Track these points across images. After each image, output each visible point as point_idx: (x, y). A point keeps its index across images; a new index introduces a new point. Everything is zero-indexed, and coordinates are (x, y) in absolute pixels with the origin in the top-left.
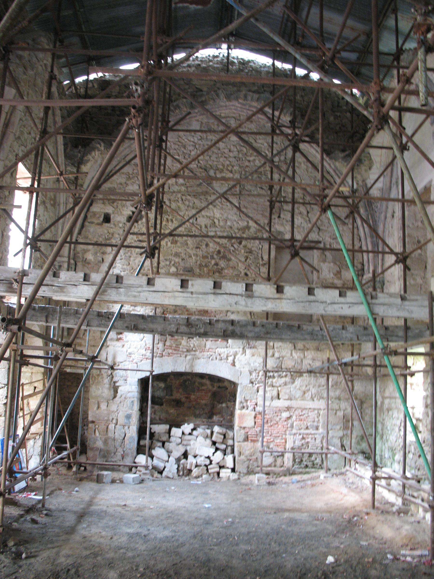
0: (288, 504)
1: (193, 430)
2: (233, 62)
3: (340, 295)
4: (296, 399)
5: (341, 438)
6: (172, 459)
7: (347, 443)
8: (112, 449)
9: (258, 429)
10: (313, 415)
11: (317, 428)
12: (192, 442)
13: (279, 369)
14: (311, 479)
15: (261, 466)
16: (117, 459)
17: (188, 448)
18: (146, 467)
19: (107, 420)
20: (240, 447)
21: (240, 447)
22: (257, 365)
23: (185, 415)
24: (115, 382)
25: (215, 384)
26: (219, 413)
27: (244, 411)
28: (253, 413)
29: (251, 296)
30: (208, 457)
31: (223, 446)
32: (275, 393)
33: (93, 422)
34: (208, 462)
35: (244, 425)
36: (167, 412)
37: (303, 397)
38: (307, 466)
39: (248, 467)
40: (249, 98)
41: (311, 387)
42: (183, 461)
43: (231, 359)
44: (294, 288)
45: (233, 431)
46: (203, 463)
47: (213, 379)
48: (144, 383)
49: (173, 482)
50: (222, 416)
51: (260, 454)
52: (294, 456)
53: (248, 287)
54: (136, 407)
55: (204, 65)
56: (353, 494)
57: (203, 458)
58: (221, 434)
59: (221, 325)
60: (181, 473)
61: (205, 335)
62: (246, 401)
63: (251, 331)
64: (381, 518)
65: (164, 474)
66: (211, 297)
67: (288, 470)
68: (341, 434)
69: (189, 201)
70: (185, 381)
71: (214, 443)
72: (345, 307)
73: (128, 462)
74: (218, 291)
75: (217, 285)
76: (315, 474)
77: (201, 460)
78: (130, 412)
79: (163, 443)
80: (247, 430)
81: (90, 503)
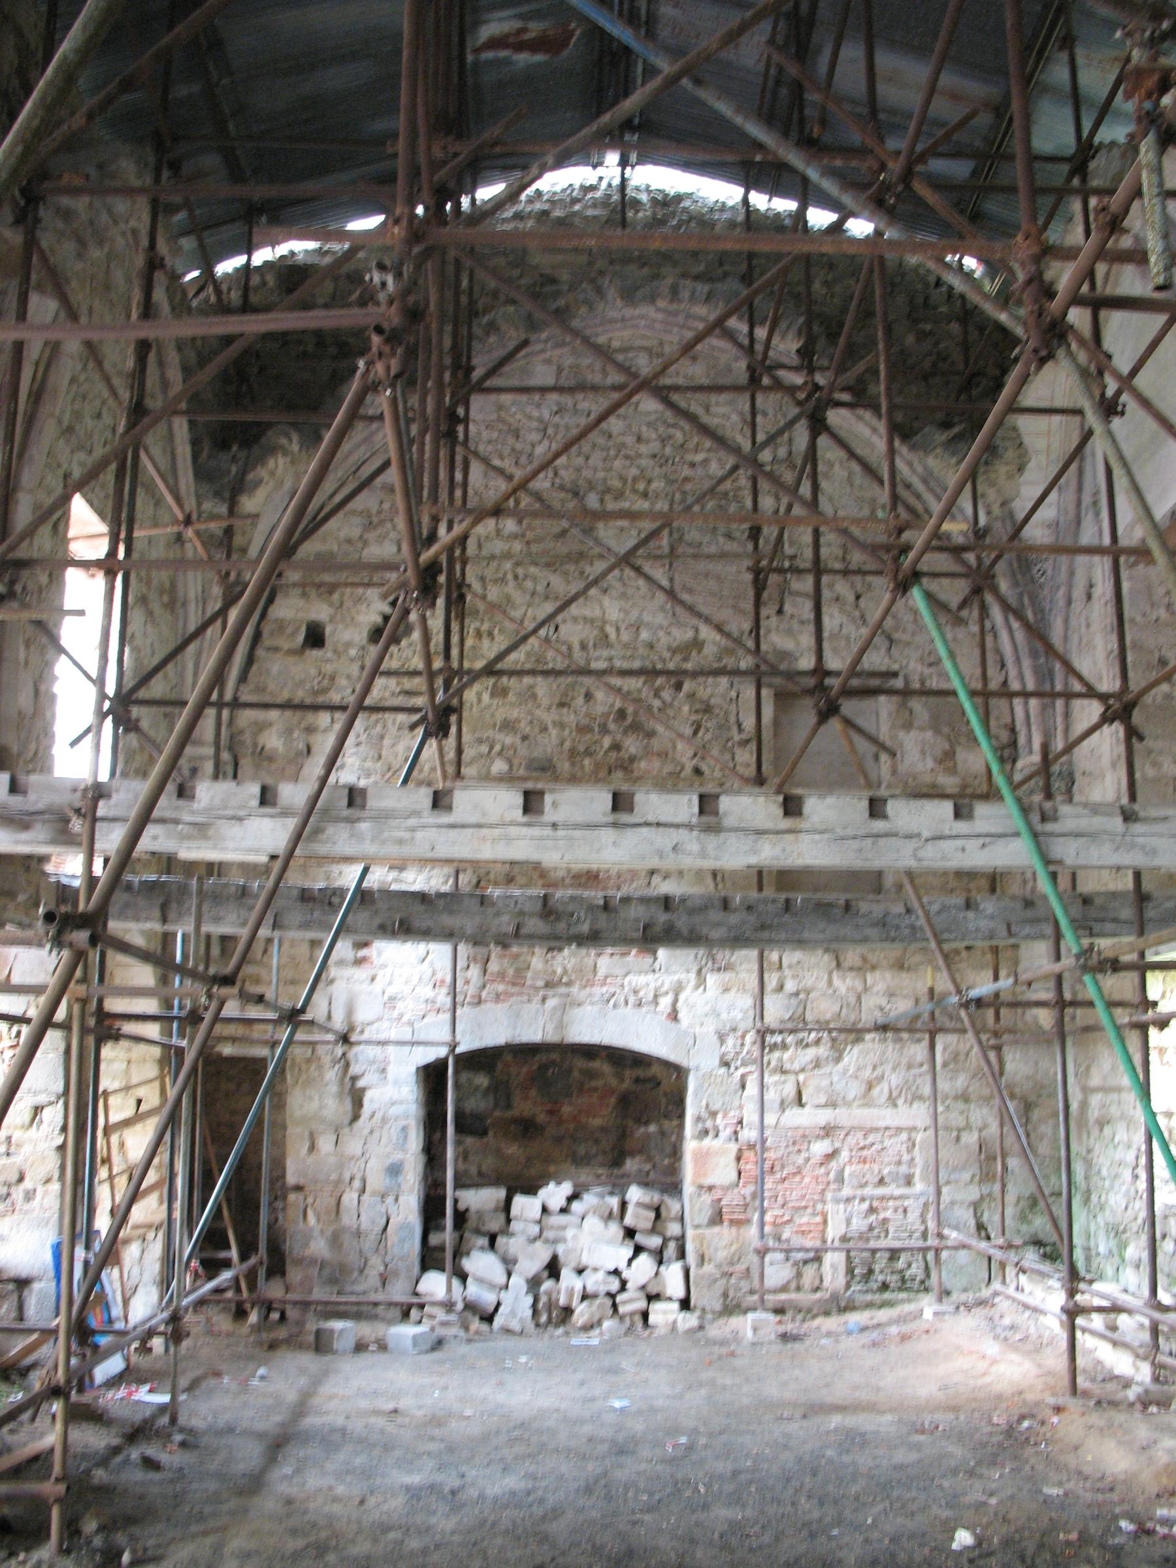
0: (840, 1392)
1: (571, 1199)
3: (958, 815)
4: (848, 1104)
5: (976, 1206)
6: (518, 1282)
8: (353, 1259)
9: (748, 1190)
10: (895, 1145)
11: (909, 1181)
13: (797, 1025)
14: (900, 1320)
16: (366, 1286)
17: (560, 1249)
18: (449, 1306)
19: (338, 1182)
21: (701, 1239)
23: (547, 1160)
24: (354, 1079)
25: (627, 1073)
26: (641, 1150)
27: (708, 1142)
28: (733, 1148)
29: (714, 829)
30: (616, 1272)
31: (657, 1239)
32: (789, 1090)
33: (299, 1188)
34: (615, 1285)
36: (498, 1153)
38: (885, 1287)
39: (725, 1295)
40: (685, 294)
41: (888, 1068)
42: (547, 1285)
43: (665, 1002)
44: (830, 800)
45: (680, 1198)
46: (603, 1289)
48: (432, 1077)
49: (522, 1343)
50: (649, 1159)
51: (755, 1259)
52: (848, 1258)
53: (707, 804)
54: (415, 1141)
55: (558, 213)
56: (1014, 1357)
57: (600, 1275)
58: (647, 1207)
59: (636, 912)
60: (544, 1318)
61: (593, 939)
62: (714, 1114)
63: (718, 925)
65: (498, 1321)
66: (608, 835)
67: (835, 1297)
68: (974, 1193)
69: (535, 579)
70: (543, 1068)
71: (630, 1233)
72: (974, 844)
73: (398, 1292)
74: (624, 818)
75: (621, 803)
76: (908, 1308)
77: (596, 1281)
78: (398, 1156)
81: (301, 1409)
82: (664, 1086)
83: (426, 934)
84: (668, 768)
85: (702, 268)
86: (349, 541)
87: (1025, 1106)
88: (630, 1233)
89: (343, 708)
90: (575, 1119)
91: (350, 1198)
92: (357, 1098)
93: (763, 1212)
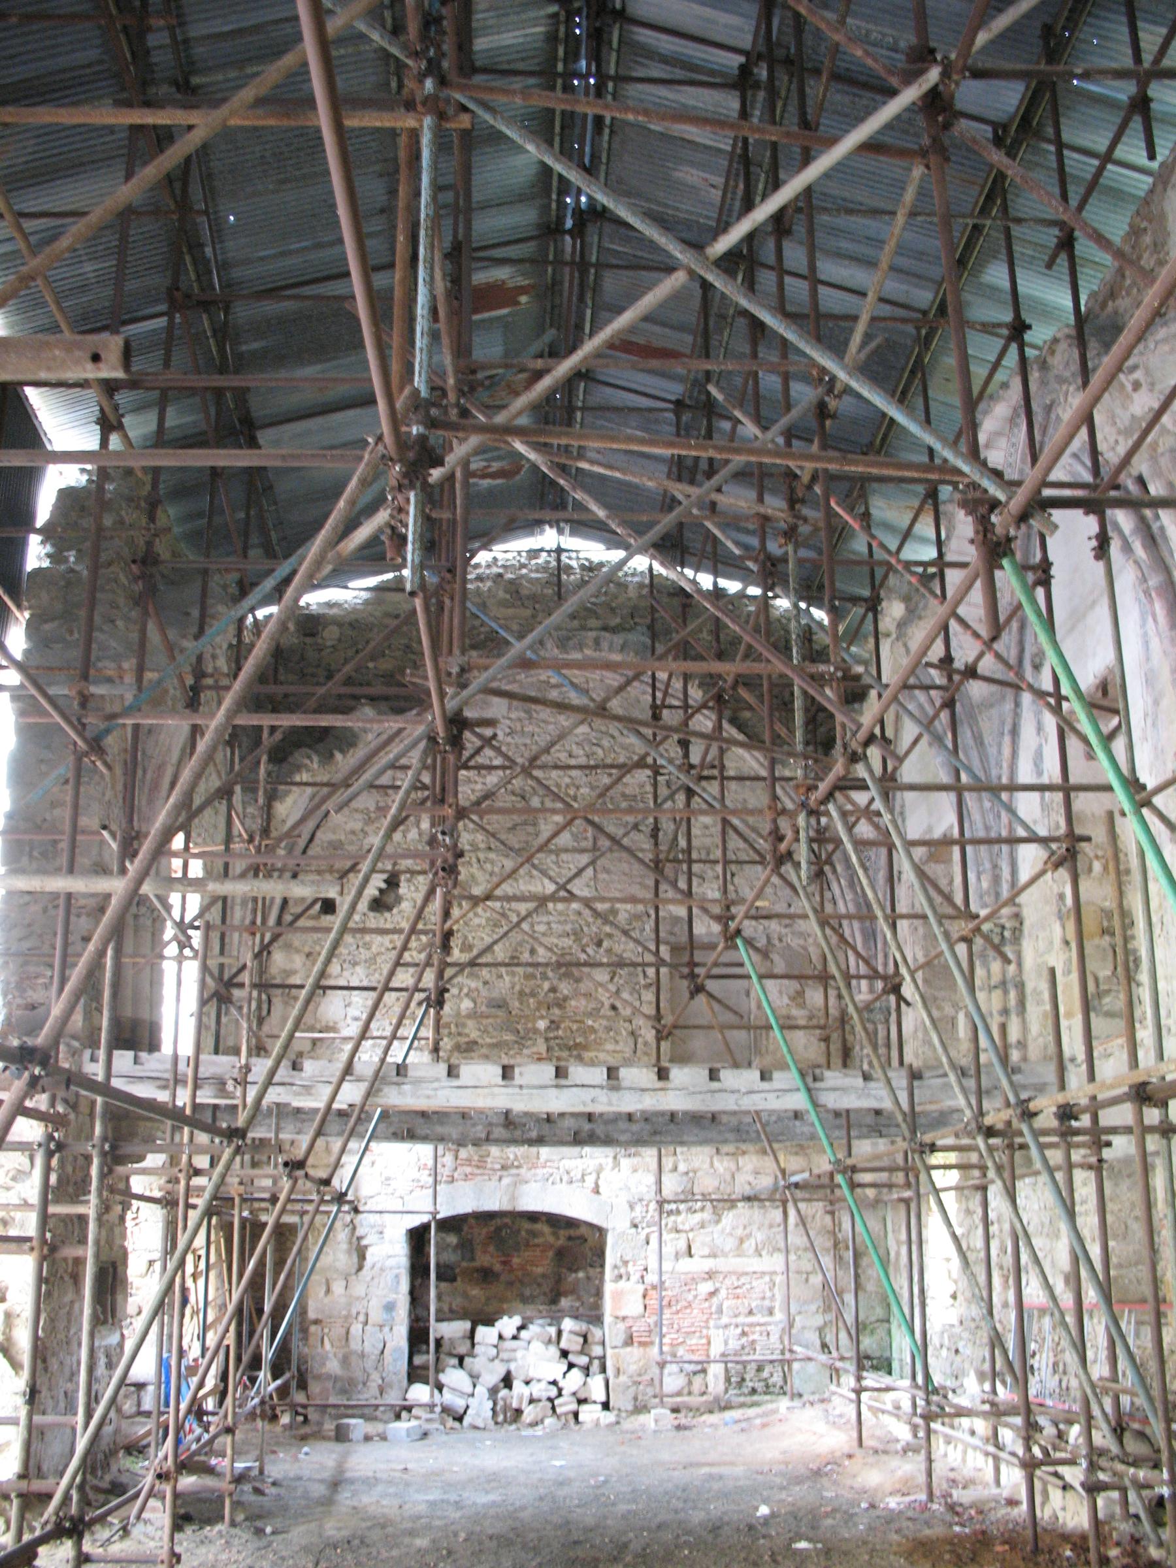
0: (713, 1456)
1: (522, 1328)
2: (570, 567)
3: (763, 1078)
4: (725, 1255)
5: (821, 1330)
6: (481, 1391)
7: (830, 1338)
8: (359, 1375)
9: (652, 1320)
10: (761, 1285)
11: (771, 1312)
12: (519, 1354)
13: (687, 1197)
14: (765, 1415)
15: (660, 1396)
16: (368, 1395)
18: (431, 1407)
19: (347, 1317)
20: (617, 1357)
21: (617, 1357)
22: (644, 1189)
23: (503, 1300)
24: (359, 1239)
25: (562, 1233)
26: (573, 1291)
27: (622, 1284)
28: (641, 1288)
30: (554, 1383)
31: (584, 1357)
32: (682, 1245)
33: (317, 1322)
34: (553, 1392)
35: (622, 1313)
36: (465, 1295)
37: (739, 1251)
38: (754, 1391)
40: (605, 645)
41: (755, 1228)
42: (504, 1393)
43: (590, 1181)
44: (686, 1070)
46: (544, 1395)
47: (556, 1221)
48: (418, 1237)
49: (486, 1434)
50: (579, 1298)
51: (656, 1370)
52: (727, 1370)
53: (612, 1073)
54: (404, 1286)
55: (510, 576)
56: (836, 1433)
57: (543, 1385)
59: (569, 1123)
60: (501, 1418)
61: (540, 1141)
62: (626, 1263)
63: (624, 1132)
64: (871, 1459)
65: (467, 1420)
66: (553, 1092)
67: (717, 1400)
68: (819, 1320)
69: (492, 862)
70: (498, 1229)
71: (564, 1354)
72: (771, 1096)
73: (393, 1398)
74: (563, 1082)
75: (560, 1073)
76: (770, 1406)
77: (541, 1390)
79: (461, 1360)
80: (629, 1323)
81: (340, 1469)
82: (590, 1242)
83: (425, 1139)
84: (592, 1005)
85: (618, 620)
86: (353, 832)
87: (855, 1256)
88: (564, 1354)
89: (374, 989)
90: (522, 1267)
91: (356, 1329)
92: (361, 1253)
93: (662, 1336)
